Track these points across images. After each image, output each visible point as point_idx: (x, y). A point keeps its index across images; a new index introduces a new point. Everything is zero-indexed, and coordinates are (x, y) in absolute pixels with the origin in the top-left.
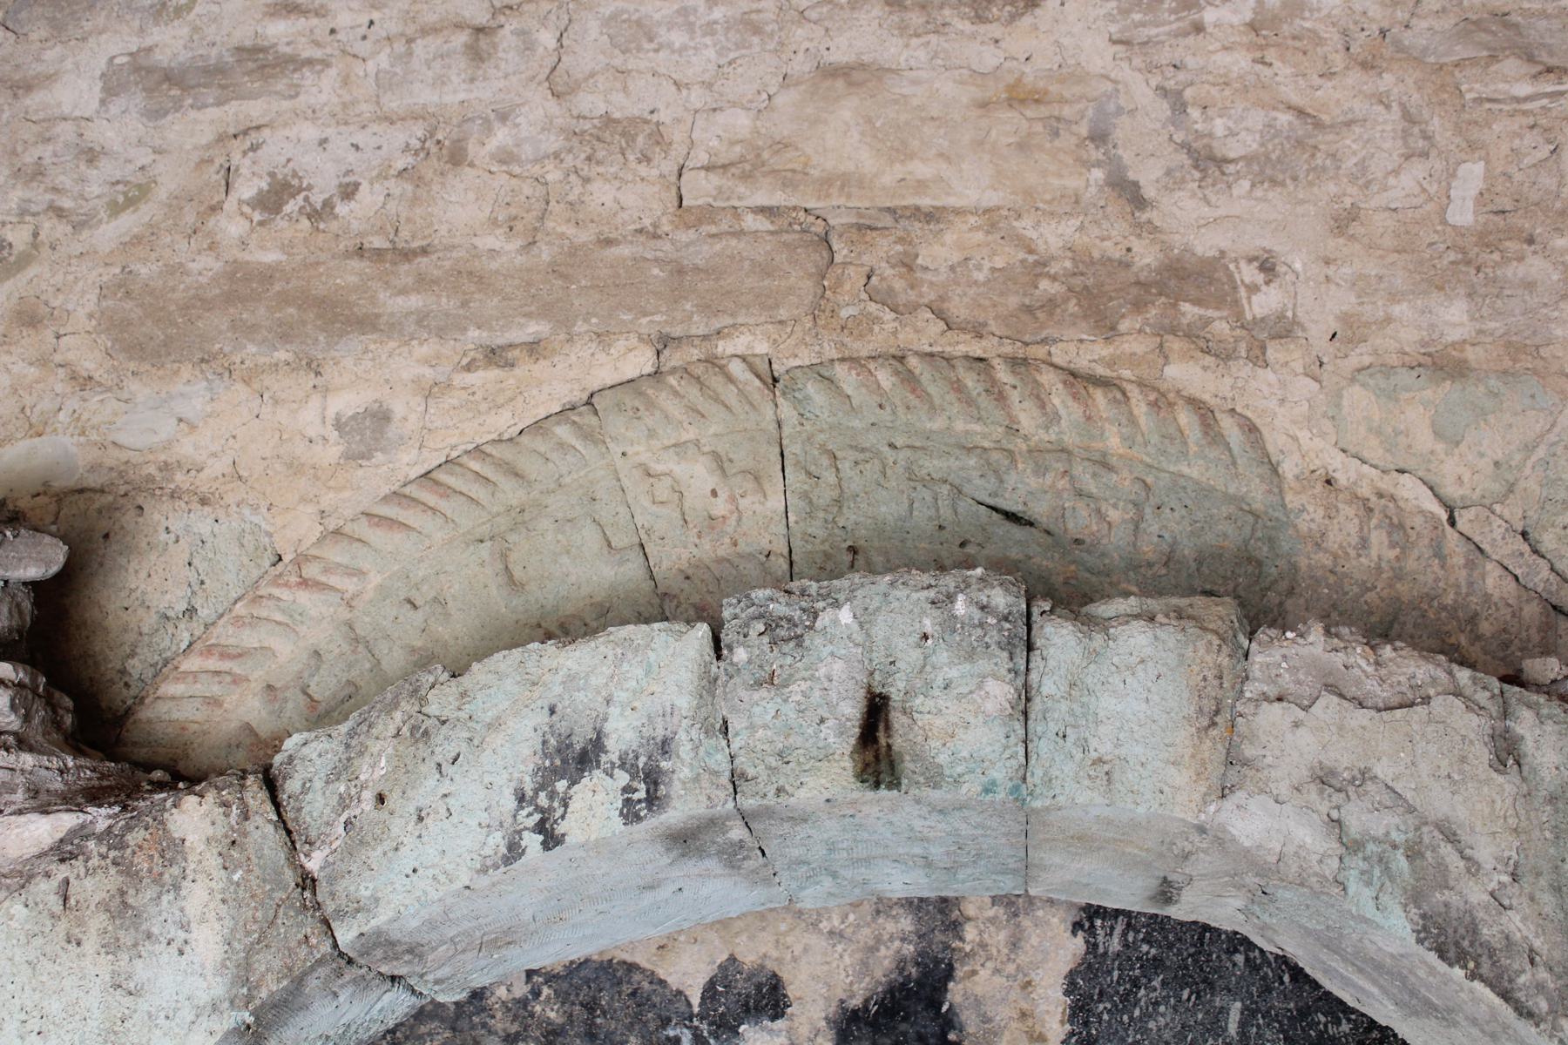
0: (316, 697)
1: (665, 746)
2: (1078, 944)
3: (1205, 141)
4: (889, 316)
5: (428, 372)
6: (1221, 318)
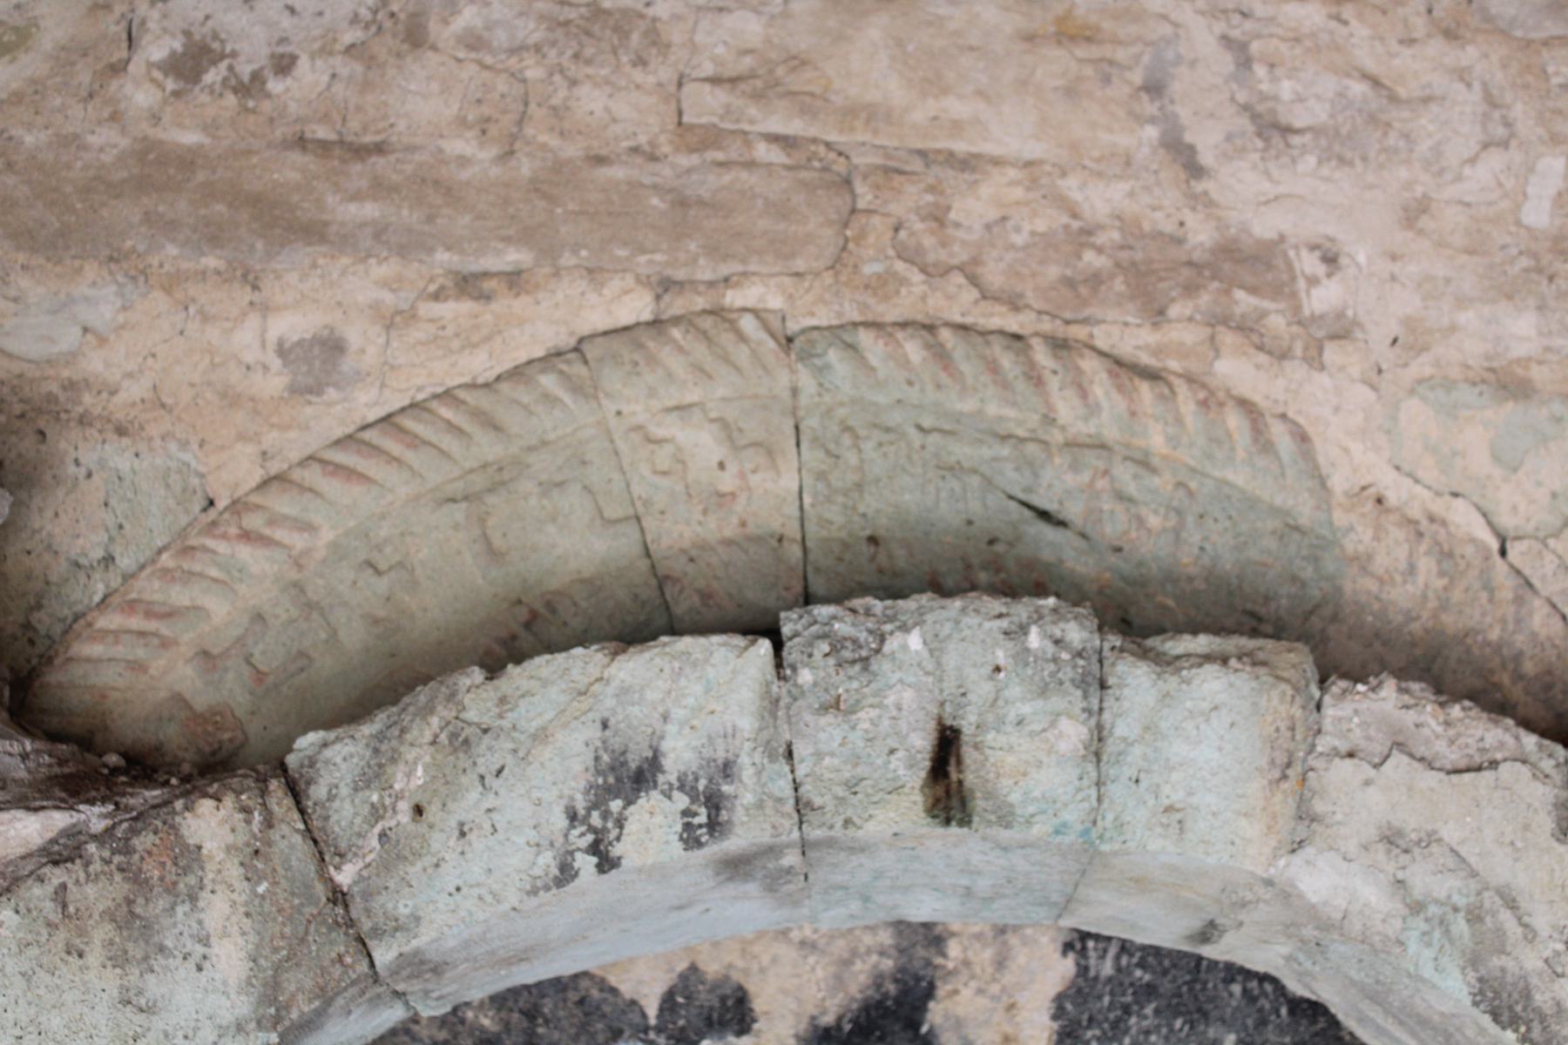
0: (262, 668)
1: (727, 769)
2: (1067, 967)
3: (1270, 104)
4: (917, 277)
5: (388, 298)
6: (1277, 311)
